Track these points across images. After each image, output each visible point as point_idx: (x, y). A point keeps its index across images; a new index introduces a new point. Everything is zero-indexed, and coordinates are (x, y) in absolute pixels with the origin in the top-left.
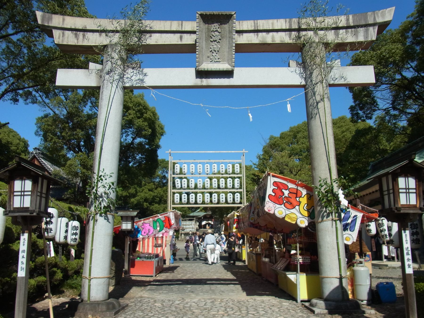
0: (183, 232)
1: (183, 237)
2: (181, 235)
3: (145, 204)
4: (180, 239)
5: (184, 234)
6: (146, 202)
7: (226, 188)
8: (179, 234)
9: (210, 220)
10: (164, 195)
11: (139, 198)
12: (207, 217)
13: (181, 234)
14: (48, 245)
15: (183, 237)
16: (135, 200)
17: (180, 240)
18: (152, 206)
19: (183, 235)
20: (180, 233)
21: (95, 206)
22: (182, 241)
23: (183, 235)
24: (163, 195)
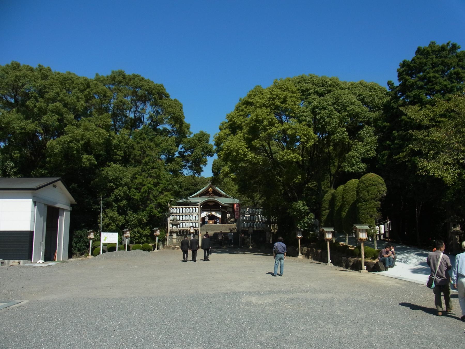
0: (175, 228)
1: (175, 241)
2: (171, 235)
3: (85, 156)
4: (167, 243)
5: (177, 233)
6: (89, 153)
7: (179, 213)
8: (166, 232)
9: (214, 211)
10: (135, 145)
11: (68, 139)
12: (209, 205)
13: (171, 233)
14: (432, 249)
15: (175, 241)
16: (59, 143)
17: (169, 247)
18: (107, 168)
19: (175, 236)
20: (169, 229)
21: (136, 290)
22: (173, 248)
23: (175, 236)
24: (132, 147)
